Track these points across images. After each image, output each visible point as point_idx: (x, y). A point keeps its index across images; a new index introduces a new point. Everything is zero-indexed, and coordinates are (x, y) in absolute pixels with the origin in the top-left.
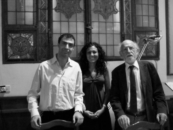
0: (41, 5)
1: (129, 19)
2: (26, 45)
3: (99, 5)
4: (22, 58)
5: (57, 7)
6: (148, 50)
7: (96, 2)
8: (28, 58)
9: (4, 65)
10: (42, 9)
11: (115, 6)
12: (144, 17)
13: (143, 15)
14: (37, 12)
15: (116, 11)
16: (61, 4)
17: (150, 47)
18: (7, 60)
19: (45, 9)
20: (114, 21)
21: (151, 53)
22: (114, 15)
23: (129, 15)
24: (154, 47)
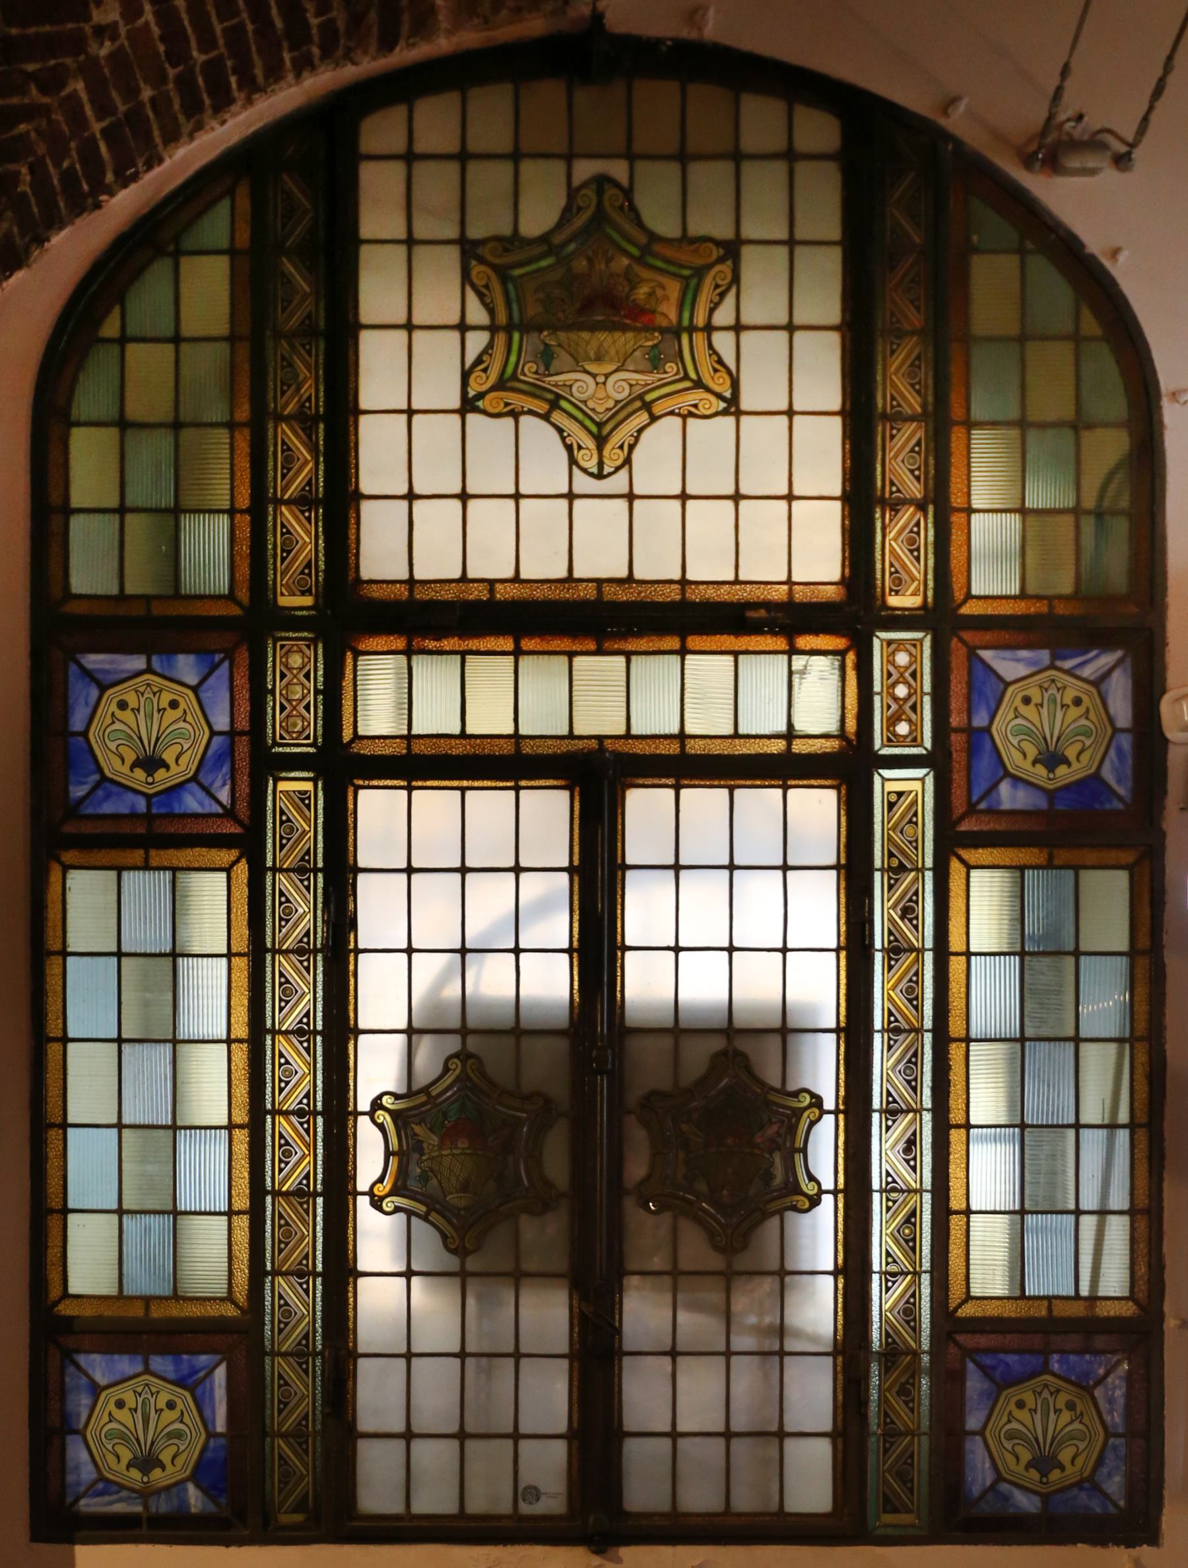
0: (281, 1170)
1: (910, 1244)
2: (182, 1426)
3: (682, 1155)
4: (153, 1510)
5: (449, 1230)
6: (1062, 1468)
7: (323, 8)
8: (193, 1510)
9: (35, 1545)
10: (287, 1194)
11: (804, 1151)
12: (1084, 1133)
13: (1083, 1121)
14: (256, 1214)
15: (810, 1189)
16: (415, 1156)
17: (1082, 1446)
18: (1153, 1539)
19: (301, 1194)
20: (789, 1266)
21: (1083, 1495)
22: (790, 1215)
23: (911, 1218)
24: (1115, 1448)
